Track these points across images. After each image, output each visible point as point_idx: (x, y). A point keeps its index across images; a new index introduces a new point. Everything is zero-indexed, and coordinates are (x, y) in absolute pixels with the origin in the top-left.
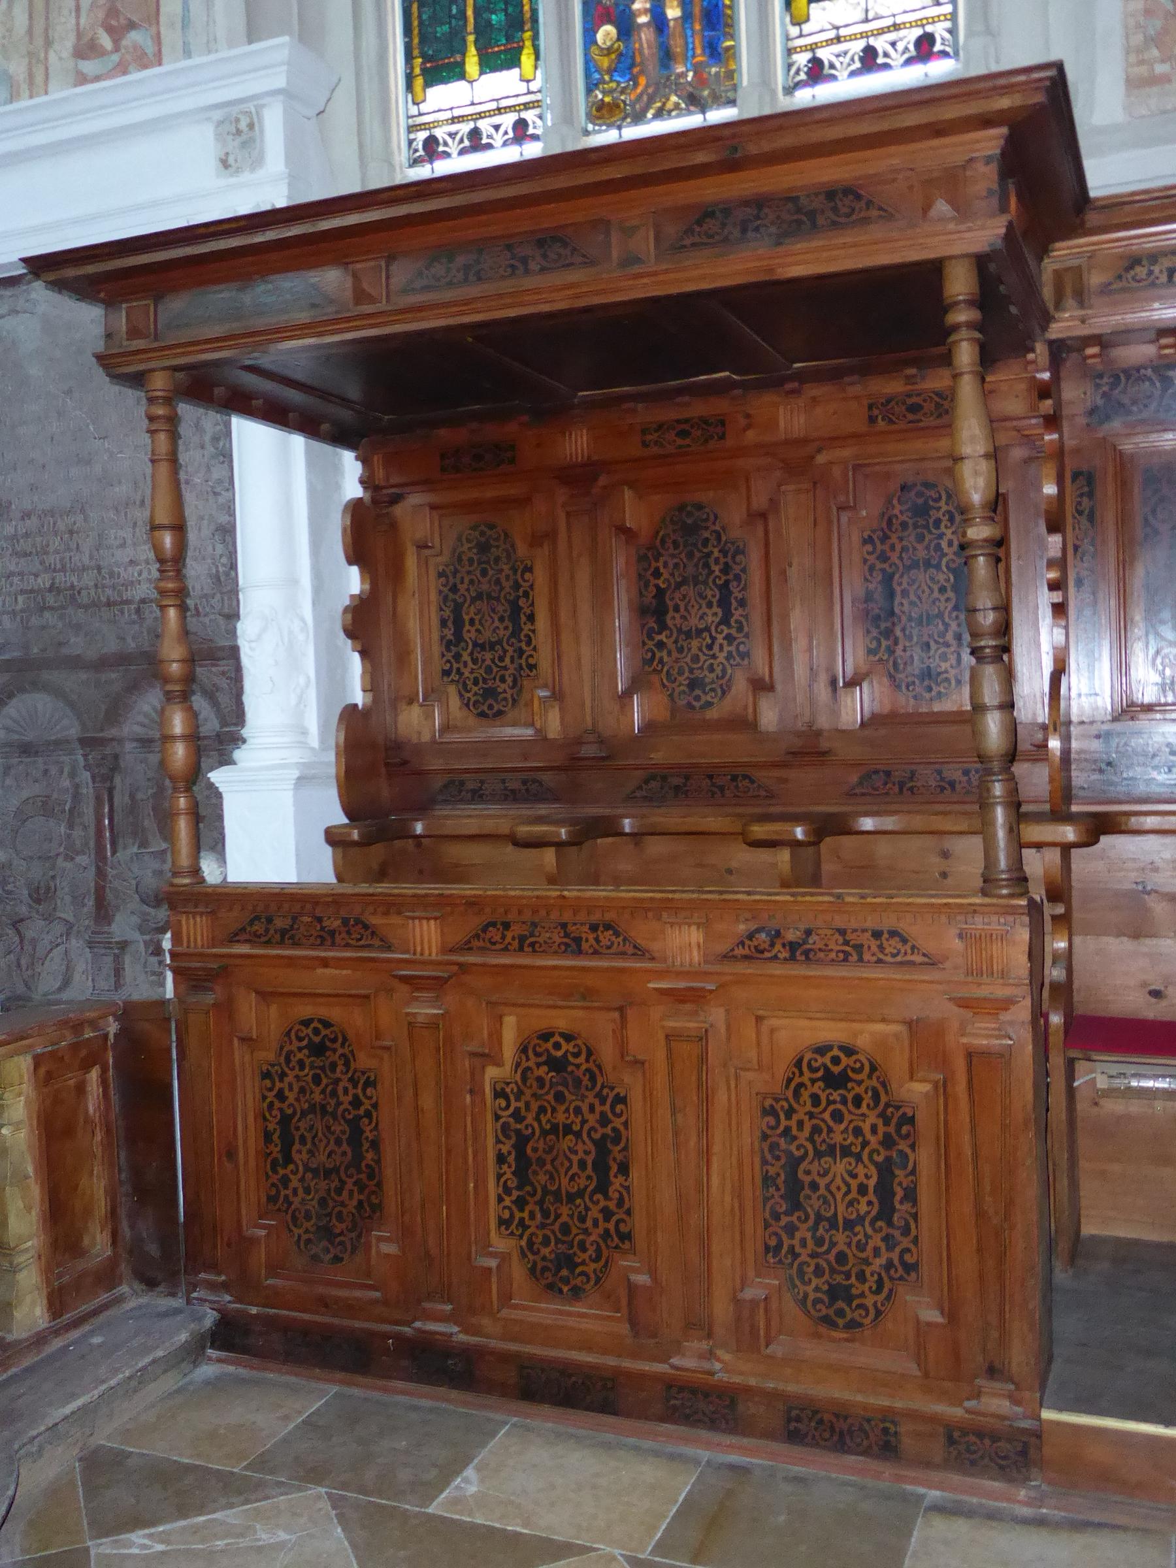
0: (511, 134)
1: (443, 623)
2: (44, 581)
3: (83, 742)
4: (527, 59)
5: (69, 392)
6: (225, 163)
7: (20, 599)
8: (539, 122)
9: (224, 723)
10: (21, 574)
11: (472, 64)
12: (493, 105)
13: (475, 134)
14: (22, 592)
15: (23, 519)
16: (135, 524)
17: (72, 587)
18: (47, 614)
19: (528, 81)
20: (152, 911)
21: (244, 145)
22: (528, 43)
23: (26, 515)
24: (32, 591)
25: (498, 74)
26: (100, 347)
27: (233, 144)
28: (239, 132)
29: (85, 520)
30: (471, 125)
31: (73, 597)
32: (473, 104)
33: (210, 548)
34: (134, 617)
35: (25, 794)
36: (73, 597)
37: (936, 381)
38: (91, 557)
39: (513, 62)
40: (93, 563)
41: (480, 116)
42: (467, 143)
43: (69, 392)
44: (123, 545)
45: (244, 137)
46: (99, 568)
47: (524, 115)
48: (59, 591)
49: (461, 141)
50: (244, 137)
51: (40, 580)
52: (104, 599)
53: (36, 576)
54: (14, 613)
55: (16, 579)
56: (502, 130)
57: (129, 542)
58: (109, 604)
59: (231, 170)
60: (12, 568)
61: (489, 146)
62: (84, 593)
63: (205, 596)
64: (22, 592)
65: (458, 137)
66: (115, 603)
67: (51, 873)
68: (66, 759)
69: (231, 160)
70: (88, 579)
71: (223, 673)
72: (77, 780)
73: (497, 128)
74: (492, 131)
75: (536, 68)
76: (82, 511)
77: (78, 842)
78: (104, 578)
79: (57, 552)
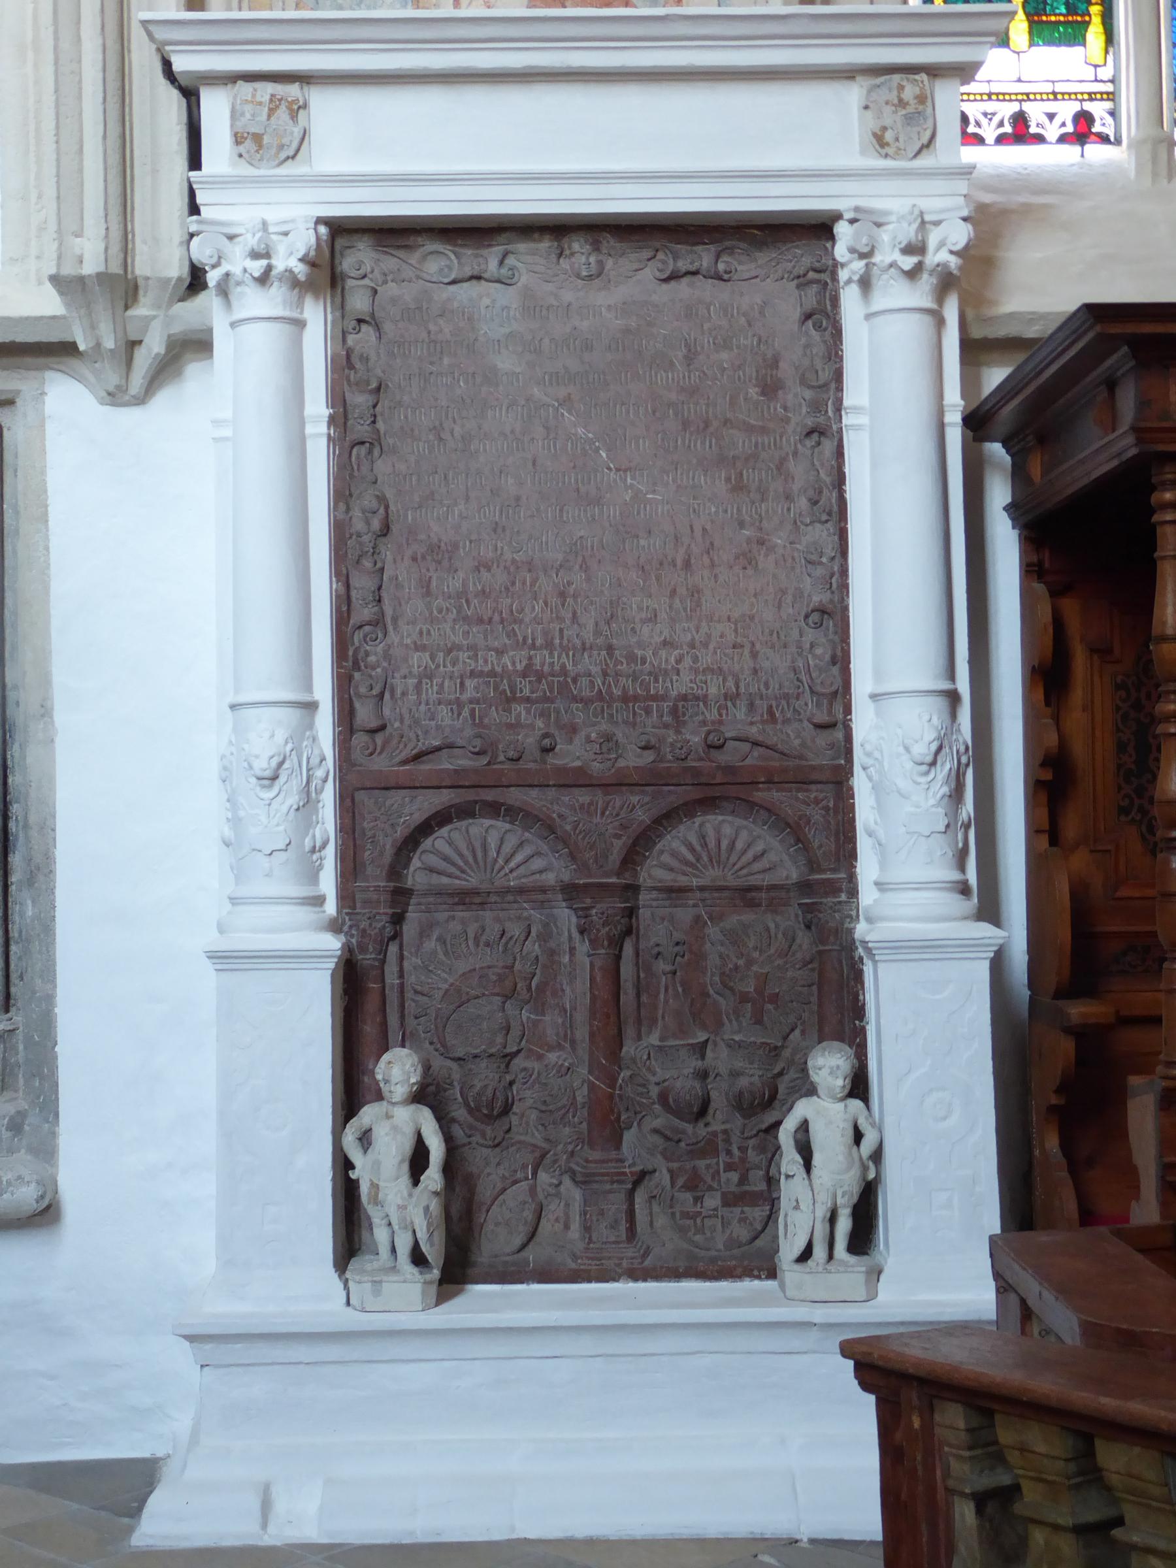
0: (1070, 128)
1: (1121, 747)
2: (513, 661)
3: (571, 891)
4: (1095, 34)
5: (567, 401)
6: (879, 139)
7: (470, 684)
8: (1109, 120)
9: (813, 865)
10: (473, 648)
11: (1019, 28)
12: (1048, 88)
13: (1020, 119)
14: (472, 674)
15: (477, 569)
16: (674, 592)
17: (564, 671)
18: (519, 709)
19: (1096, 66)
20: (689, 1128)
21: (909, 119)
22: (1096, 20)
23: (482, 566)
24: (493, 674)
25: (1054, 49)
26: (53, 271)
27: (890, 117)
28: (902, 103)
29: (588, 579)
30: (1014, 107)
31: (563, 686)
32: (1019, 80)
33: (795, 634)
34: (667, 719)
35: (462, 966)
36: (563, 686)
37: (825, 396)
38: (597, 633)
39: (1074, 34)
40: (600, 641)
41: (1027, 97)
42: (1008, 129)
43: (567, 401)
44: (653, 619)
45: (910, 109)
46: (610, 649)
47: (1088, 106)
48: (540, 676)
49: (1001, 124)
50: (910, 109)
51: (506, 660)
52: (617, 692)
53: (500, 652)
54: (459, 703)
55: (463, 656)
56: (1058, 121)
57: (662, 616)
58: (625, 699)
59: (890, 151)
60: (458, 639)
61: (1039, 139)
62: (584, 681)
63: (786, 697)
64: (472, 674)
65: (996, 120)
66: (636, 698)
67: (508, 1078)
68: (536, 915)
69: (889, 136)
70: (590, 664)
71: (817, 801)
72: (552, 944)
73: (1051, 116)
74: (1046, 120)
75: (1107, 52)
76: (585, 567)
77: (549, 1031)
78: (618, 662)
79: (537, 621)
